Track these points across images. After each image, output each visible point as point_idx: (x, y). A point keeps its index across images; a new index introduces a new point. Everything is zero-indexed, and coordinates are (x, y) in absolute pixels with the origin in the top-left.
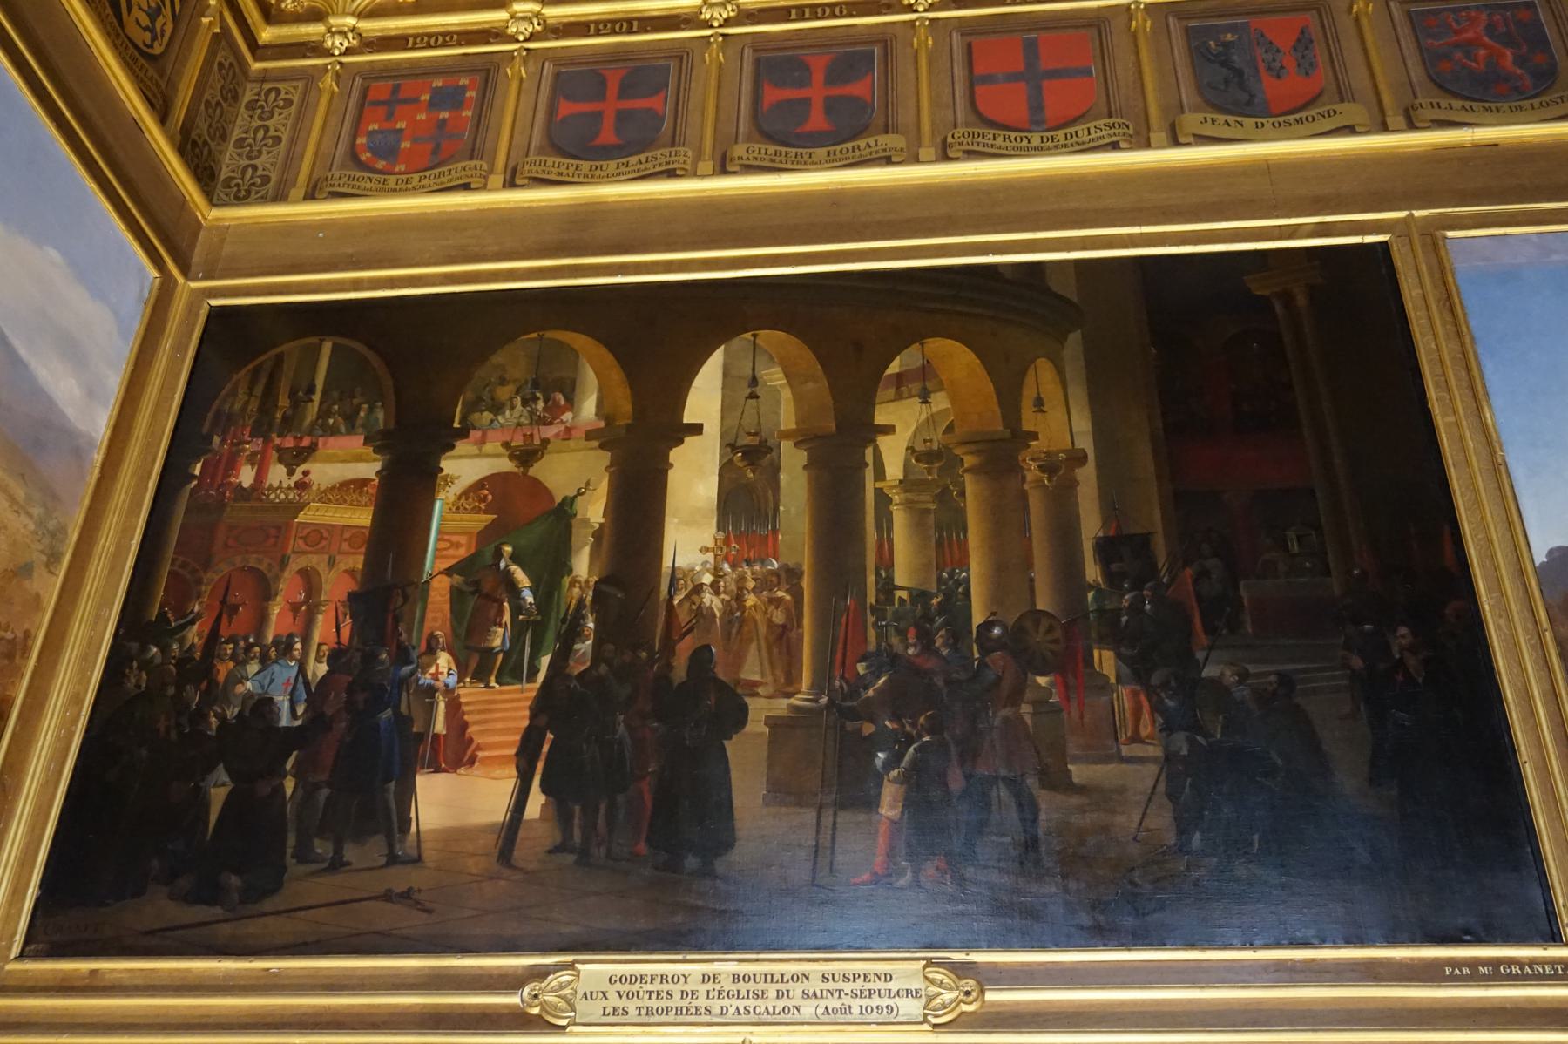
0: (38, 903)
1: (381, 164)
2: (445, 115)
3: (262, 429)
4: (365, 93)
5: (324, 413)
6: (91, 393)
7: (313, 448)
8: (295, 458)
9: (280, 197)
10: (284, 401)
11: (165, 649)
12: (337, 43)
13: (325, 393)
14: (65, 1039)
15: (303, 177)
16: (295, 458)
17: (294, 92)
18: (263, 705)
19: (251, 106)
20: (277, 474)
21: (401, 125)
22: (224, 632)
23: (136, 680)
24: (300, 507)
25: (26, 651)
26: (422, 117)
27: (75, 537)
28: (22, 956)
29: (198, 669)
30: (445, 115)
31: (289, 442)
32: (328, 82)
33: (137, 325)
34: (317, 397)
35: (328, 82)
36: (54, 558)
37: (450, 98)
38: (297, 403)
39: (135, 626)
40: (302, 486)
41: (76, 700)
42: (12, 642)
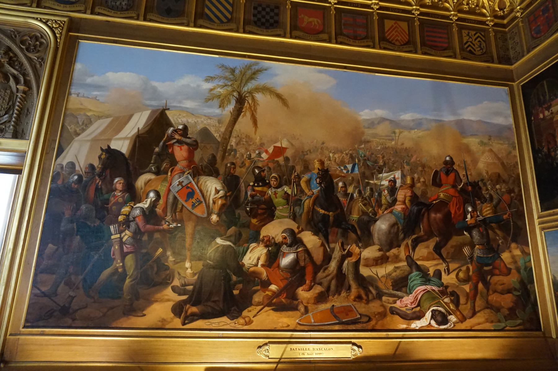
0: (540, 203)
1: (539, 36)
2: (547, 15)
3: (540, 105)
4: (529, 21)
5: (550, 97)
6: (506, 117)
7: (551, 105)
8: (548, 109)
9: (523, 56)
10: (542, 98)
11: (541, 154)
12: (518, 14)
13: (549, 92)
14: (2, 297)
15: (525, 50)
16: (548, 109)
17: (515, 30)
18: (286, 298)
19: (510, 38)
20: (547, 113)
21: (539, 24)
22: (550, 147)
23: (539, 161)
24: (554, 117)
25: (517, 164)
26: (542, 19)
27: (516, 142)
28: (542, 211)
29: (548, 155)
30: (547, 15)
31: (546, 106)
32: (521, 24)
33: (509, 99)
34: (547, 93)
35: (521, 24)
36: (514, 148)
37: (547, 10)
38: (544, 97)
39: (535, 152)
40: (552, 113)
41: (531, 168)
42: (514, 165)
